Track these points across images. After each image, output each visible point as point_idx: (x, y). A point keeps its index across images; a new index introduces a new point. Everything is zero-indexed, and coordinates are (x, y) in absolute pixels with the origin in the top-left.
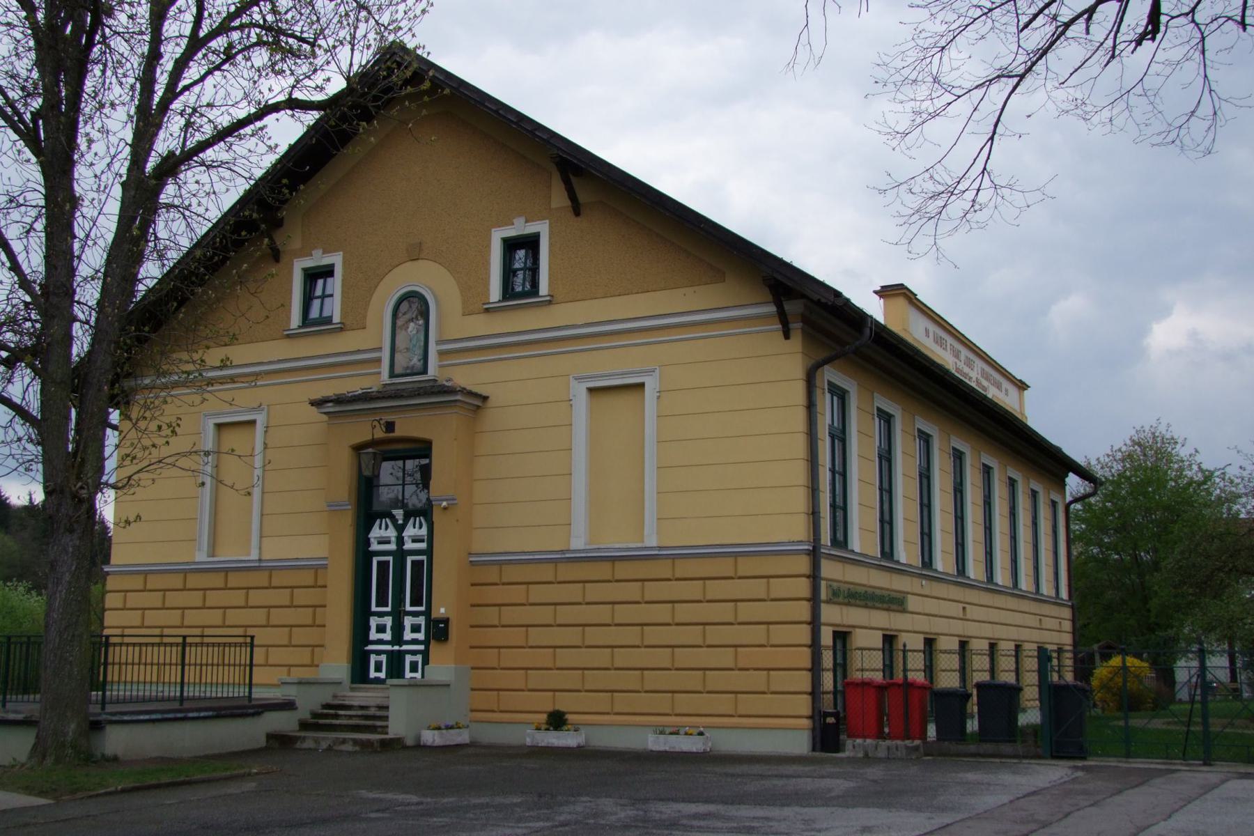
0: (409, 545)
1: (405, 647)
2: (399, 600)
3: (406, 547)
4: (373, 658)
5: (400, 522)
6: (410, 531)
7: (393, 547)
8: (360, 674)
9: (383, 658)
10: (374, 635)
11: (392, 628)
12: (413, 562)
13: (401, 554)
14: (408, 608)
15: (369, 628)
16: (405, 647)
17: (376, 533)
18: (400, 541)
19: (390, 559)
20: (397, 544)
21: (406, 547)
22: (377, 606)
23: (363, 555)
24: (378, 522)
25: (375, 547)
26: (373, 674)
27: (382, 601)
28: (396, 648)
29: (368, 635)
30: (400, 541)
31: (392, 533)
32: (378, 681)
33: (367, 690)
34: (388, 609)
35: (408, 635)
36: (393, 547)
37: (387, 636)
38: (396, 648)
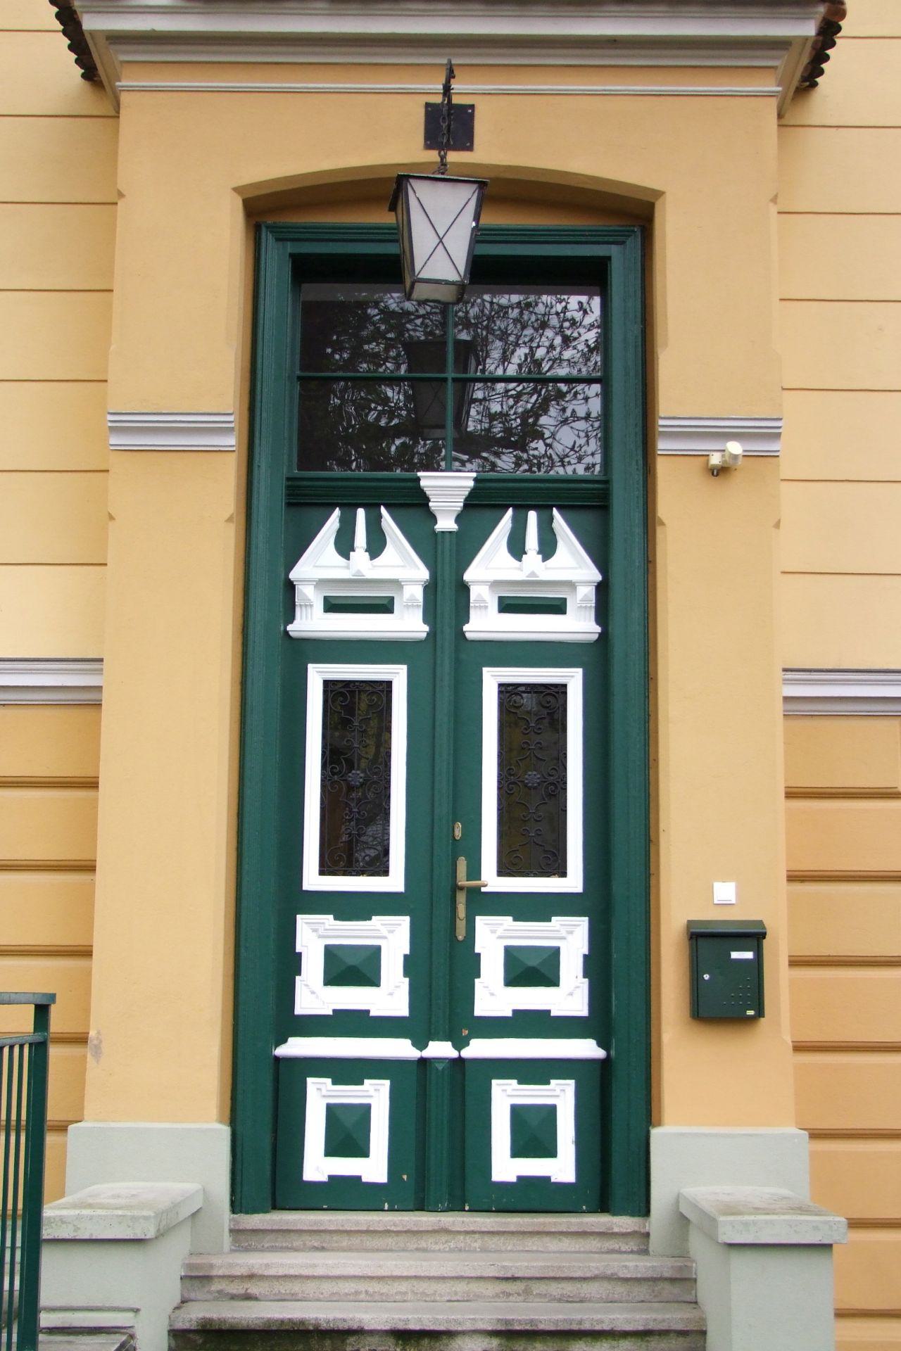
0: (486, 622)
1: (479, 1048)
2: (443, 844)
3: (298, 627)
4: (320, 1095)
5: (446, 523)
6: (491, 566)
7: (408, 622)
8: (265, 1172)
9: (376, 1095)
10: (313, 995)
11: (410, 965)
12: (330, 687)
13: (447, 655)
14: (313, 879)
15: (292, 963)
16: (479, 1048)
17: (319, 564)
18: (448, 598)
19: (398, 675)
20: (431, 611)
21: (298, 627)
22: (325, 870)
23: (269, 655)
24: (334, 521)
25: (312, 621)
26: (318, 1165)
27: (532, 845)
28: (440, 1049)
29: (287, 994)
30: (448, 598)
31: (402, 566)
32: (345, 1194)
33: (321, 1240)
34: (394, 881)
35: (493, 996)
36: (408, 622)
37: (391, 996)
38: (440, 1049)
